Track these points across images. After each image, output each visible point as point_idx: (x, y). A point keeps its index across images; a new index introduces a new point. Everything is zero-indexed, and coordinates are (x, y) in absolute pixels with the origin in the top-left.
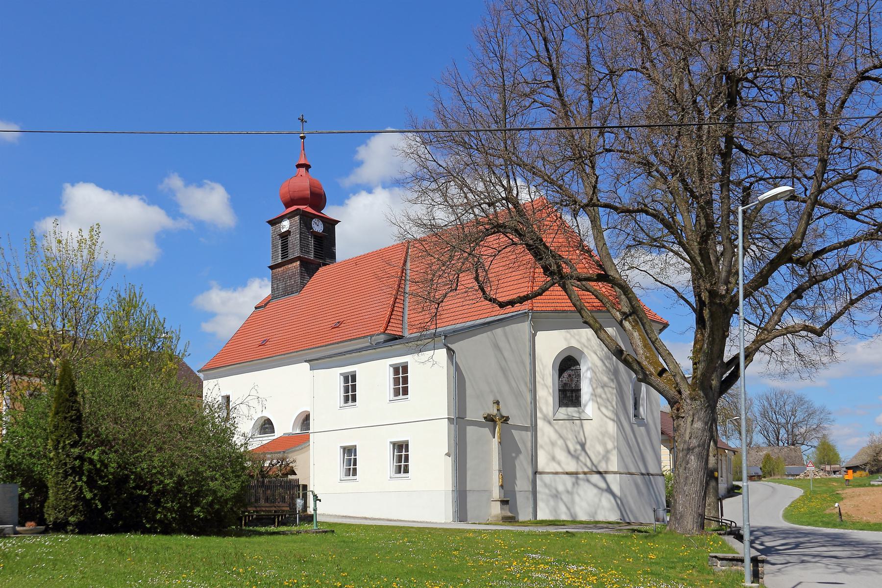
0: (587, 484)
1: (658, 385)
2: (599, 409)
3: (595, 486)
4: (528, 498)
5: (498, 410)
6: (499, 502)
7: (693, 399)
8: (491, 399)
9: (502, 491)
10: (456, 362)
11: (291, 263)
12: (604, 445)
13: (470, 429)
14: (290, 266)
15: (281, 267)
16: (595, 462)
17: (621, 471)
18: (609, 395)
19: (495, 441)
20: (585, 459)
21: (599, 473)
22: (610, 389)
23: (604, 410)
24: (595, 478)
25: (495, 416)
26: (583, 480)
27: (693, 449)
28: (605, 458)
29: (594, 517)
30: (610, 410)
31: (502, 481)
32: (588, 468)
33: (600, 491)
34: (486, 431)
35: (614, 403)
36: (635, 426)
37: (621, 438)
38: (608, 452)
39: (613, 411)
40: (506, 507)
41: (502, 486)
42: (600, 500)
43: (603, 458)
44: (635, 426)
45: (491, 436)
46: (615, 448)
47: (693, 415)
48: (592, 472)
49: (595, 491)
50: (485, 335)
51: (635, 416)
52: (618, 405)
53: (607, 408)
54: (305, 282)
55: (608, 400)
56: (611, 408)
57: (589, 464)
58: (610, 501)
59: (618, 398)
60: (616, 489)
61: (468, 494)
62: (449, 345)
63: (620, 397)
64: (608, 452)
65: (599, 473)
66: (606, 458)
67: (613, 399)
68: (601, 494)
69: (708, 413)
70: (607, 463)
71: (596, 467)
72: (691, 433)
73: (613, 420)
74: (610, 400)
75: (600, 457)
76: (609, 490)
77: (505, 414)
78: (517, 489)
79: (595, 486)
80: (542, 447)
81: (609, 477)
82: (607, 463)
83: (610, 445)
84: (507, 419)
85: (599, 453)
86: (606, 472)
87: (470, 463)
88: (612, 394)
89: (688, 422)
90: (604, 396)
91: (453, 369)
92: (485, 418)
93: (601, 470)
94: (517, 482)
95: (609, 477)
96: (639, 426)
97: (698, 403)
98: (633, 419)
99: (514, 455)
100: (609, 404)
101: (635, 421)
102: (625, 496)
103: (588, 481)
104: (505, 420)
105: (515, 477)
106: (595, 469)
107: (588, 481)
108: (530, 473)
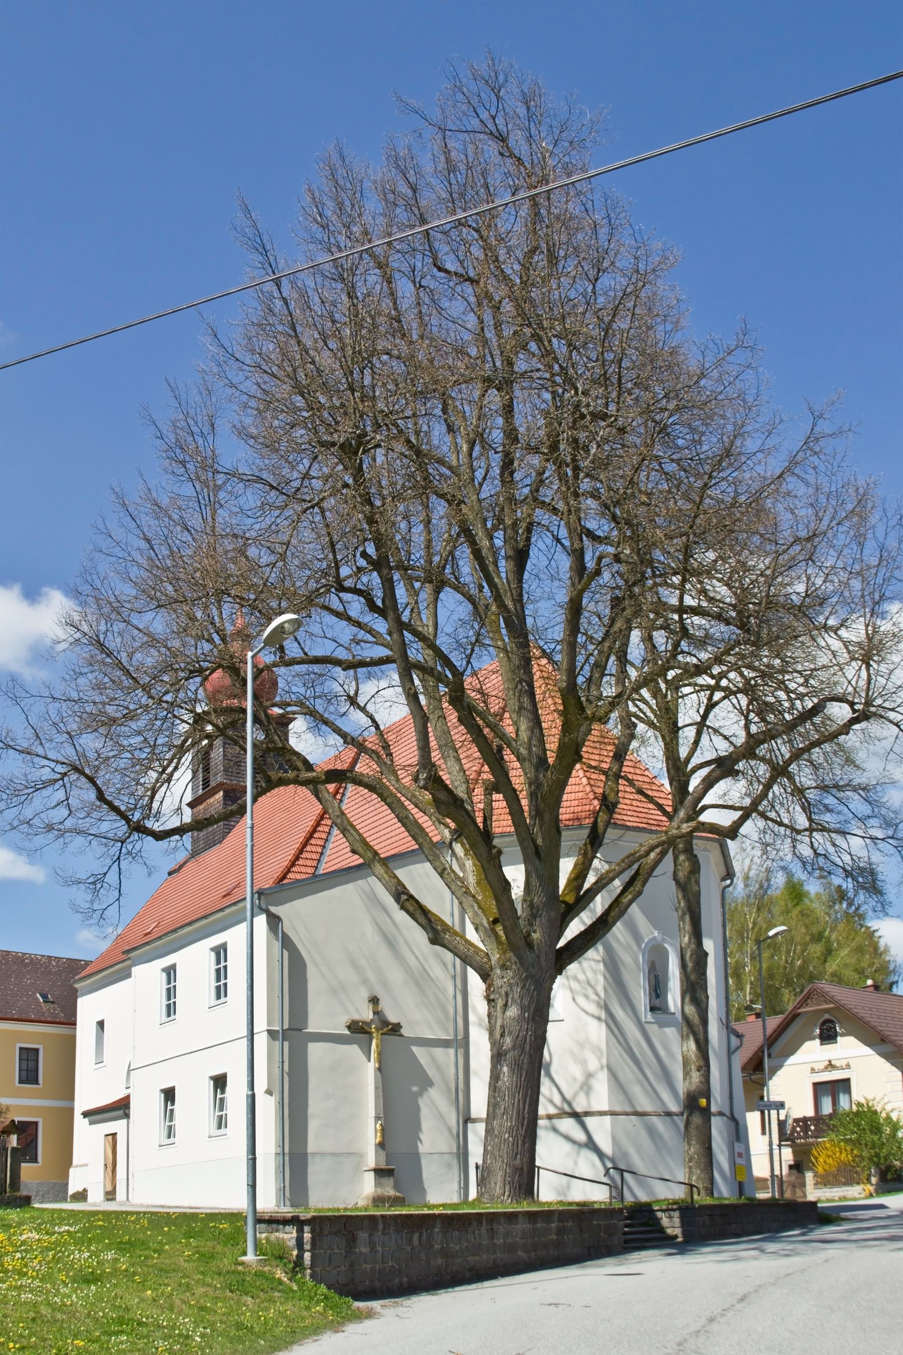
0: (552, 1135)
1: (456, 948)
2: (574, 999)
3: (568, 1138)
4: (449, 1166)
5: (376, 1013)
6: (372, 1174)
7: (504, 967)
8: (365, 994)
9: (383, 1154)
10: (283, 932)
11: (214, 795)
12: (583, 1063)
13: (315, 1051)
14: (212, 800)
15: (201, 803)
16: (568, 1096)
17: (618, 1109)
18: (590, 975)
19: (371, 1067)
20: (551, 1090)
21: (575, 1115)
22: (592, 963)
23: (581, 1000)
24: (568, 1125)
25: (368, 1024)
26: (546, 1128)
27: (506, 1054)
28: (585, 1088)
29: (565, 1195)
30: (593, 1001)
31: (383, 1136)
32: (555, 1106)
33: (576, 1147)
34: (354, 1050)
35: (600, 989)
36: (653, 1029)
37: (618, 1050)
38: (589, 1076)
39: (598, 1004)
40: (390, 1181)
41: (381, 1145)
42: (576, 1163)
43: (581, 1088)
44: (653, 1029)
45: (364, 1059)
46: (602, 1068)
47: (507, 994)
48: (562, 1114)
49: (567, 1146)
50: (350, 886)
51: (653, 1009)
52: (609, 990)
53: (587, 997)
54: (232, 823)
55: (589, 983)
56: (594, 997)
57: (557, 1099)
58: (594, 1165)
59: (610, 979)
60: (605, 1144)
61: (310, 1159)
62: (273, 909)
63: (612, 976)
64: (589, 1076)
65: (575, 1115)
66: (586, 1087)
67: (597, 981)
68: (578, 1153)
69: (528, 990)
70: (587, 1094)
71: (570, 1104)
72: (503, 1027)
73: (599, 1019)
74: (593, 983)
75: (577, 1086)
76: (591, 1145)
77: (393, 1018)
78: (422, 1149)
79: (568, 1138)
80: (476, 1073)
81: (589, 1121)
82: (587, 1094)
83: (593, 1064)
84: (395, 1029)
85: (575, 1079)
86: (587, 1114)
87: (316, 1105)
88: (595, 972)
89: (498, 1008)
90: (581, 977)
91: (277, 945)
92: (349, 1027)
93: (579, 1109)
94: (422, 1136)
95: (589, 1121)
96: (662, 1025)
97: (510, 973)
98: (646, 1016)
99: (415, 1089)
100: (590, 992)
101: (653, 1018)
102: (625, 1155)
103: (555, 1130)
104: (390, 1030)
105: (417, 1127)
106: (566, 1108)
107: (555, 1130)
108: (452, 1119)
